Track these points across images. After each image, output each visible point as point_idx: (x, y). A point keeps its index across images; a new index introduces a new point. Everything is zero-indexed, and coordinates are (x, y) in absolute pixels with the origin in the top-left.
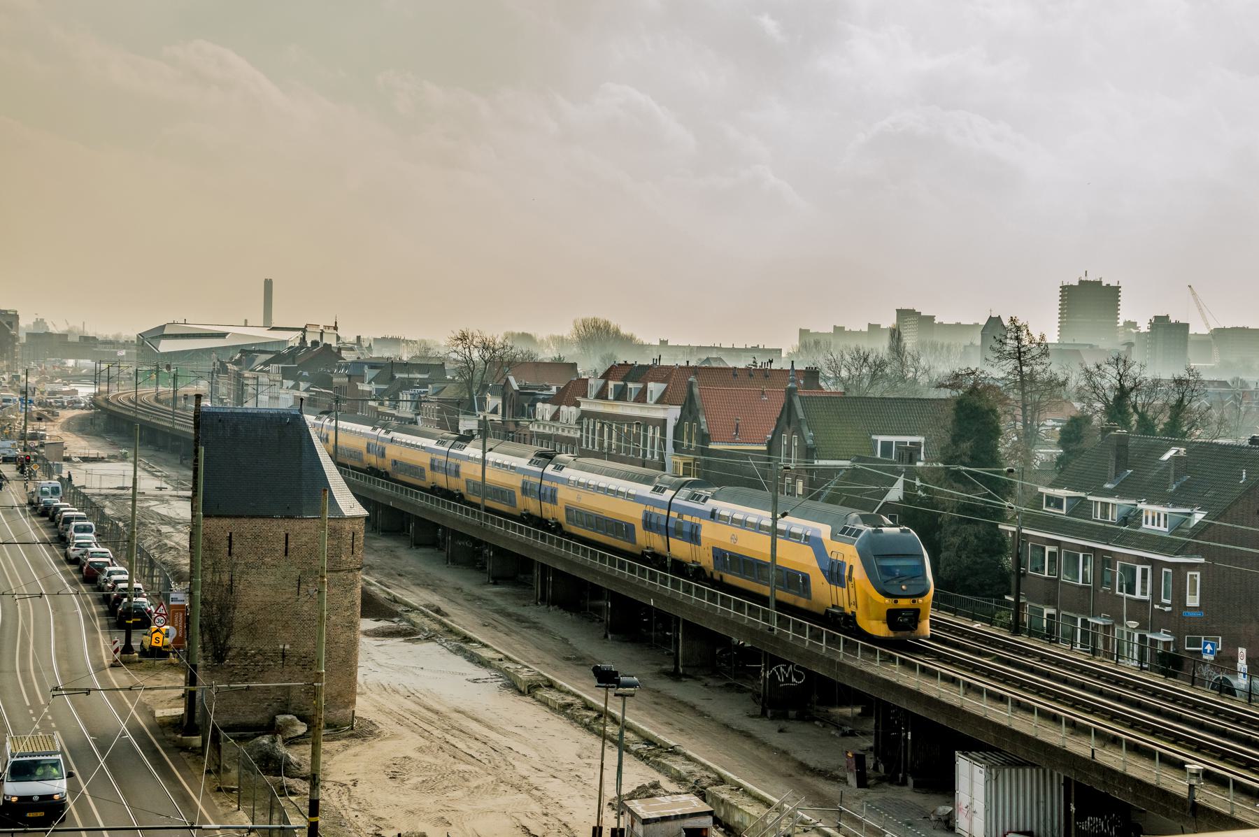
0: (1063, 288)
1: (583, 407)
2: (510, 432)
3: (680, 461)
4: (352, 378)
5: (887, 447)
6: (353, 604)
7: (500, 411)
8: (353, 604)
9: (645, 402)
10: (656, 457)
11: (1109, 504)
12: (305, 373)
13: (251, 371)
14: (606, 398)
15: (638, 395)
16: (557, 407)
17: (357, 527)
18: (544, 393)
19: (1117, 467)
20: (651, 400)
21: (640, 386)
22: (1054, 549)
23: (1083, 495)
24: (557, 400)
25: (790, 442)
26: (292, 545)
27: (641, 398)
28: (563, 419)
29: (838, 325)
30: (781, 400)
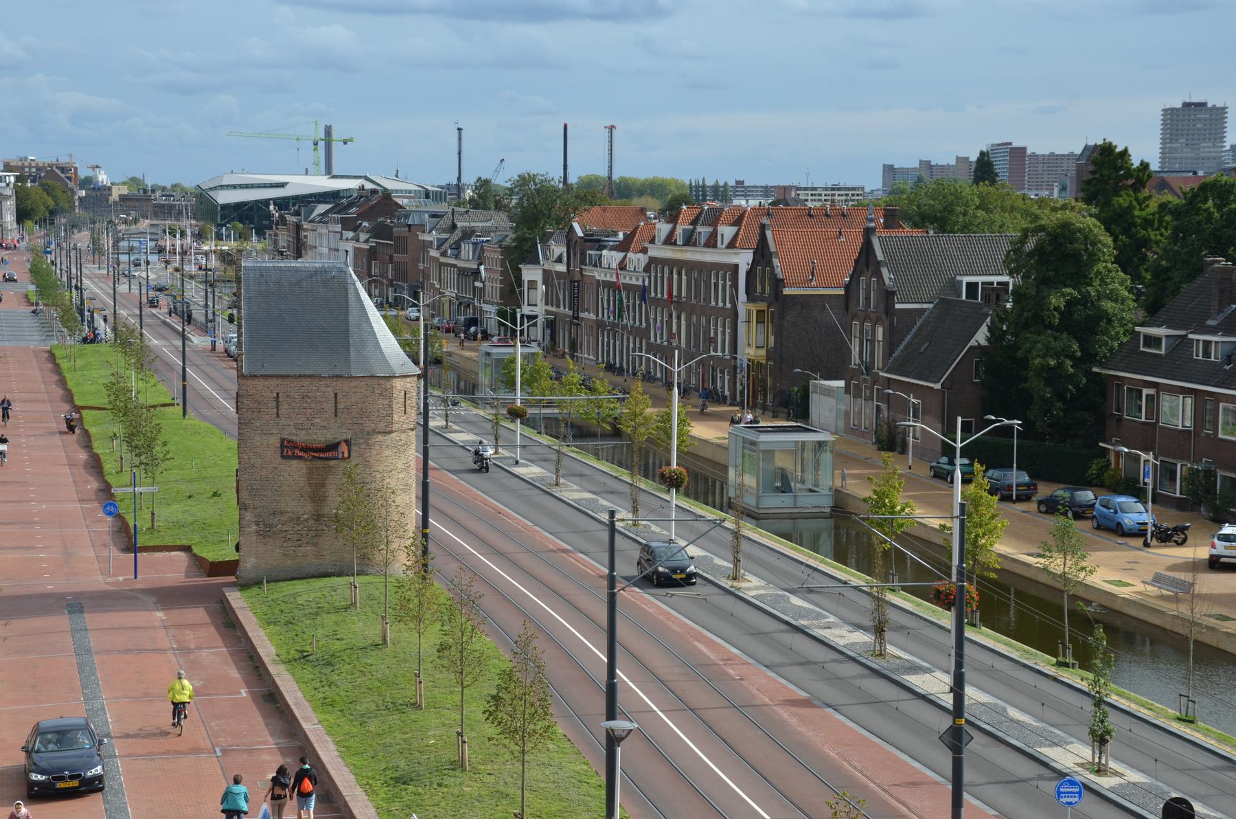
0: (1165, 110)
1: (650, 253)
2: (576, 282)
3: (754, 308)
4: (412, 228)
5: (972, 287)
6: (407, 465)
7: (565, 259)
8: (407, 465)
9: (715, 246)
10: (728, 305)
11: (1211, 342)
12: (365, 224)
13: (309, 222)
14: (675, 244)
15: (707, 240)
16: (624, 254)
17: (408, 385)
18: (610, 239)
19: (1220, 302)
20: (722, 244)
21: (710, 229)
22: (1152, 391)
23: (1183, 333)
24: (624, 246)
25: (869, 286)
26: (341, 406)
27: (711, 243)
28: (630, 267)
29: (960, 156)
30: (858, 242)
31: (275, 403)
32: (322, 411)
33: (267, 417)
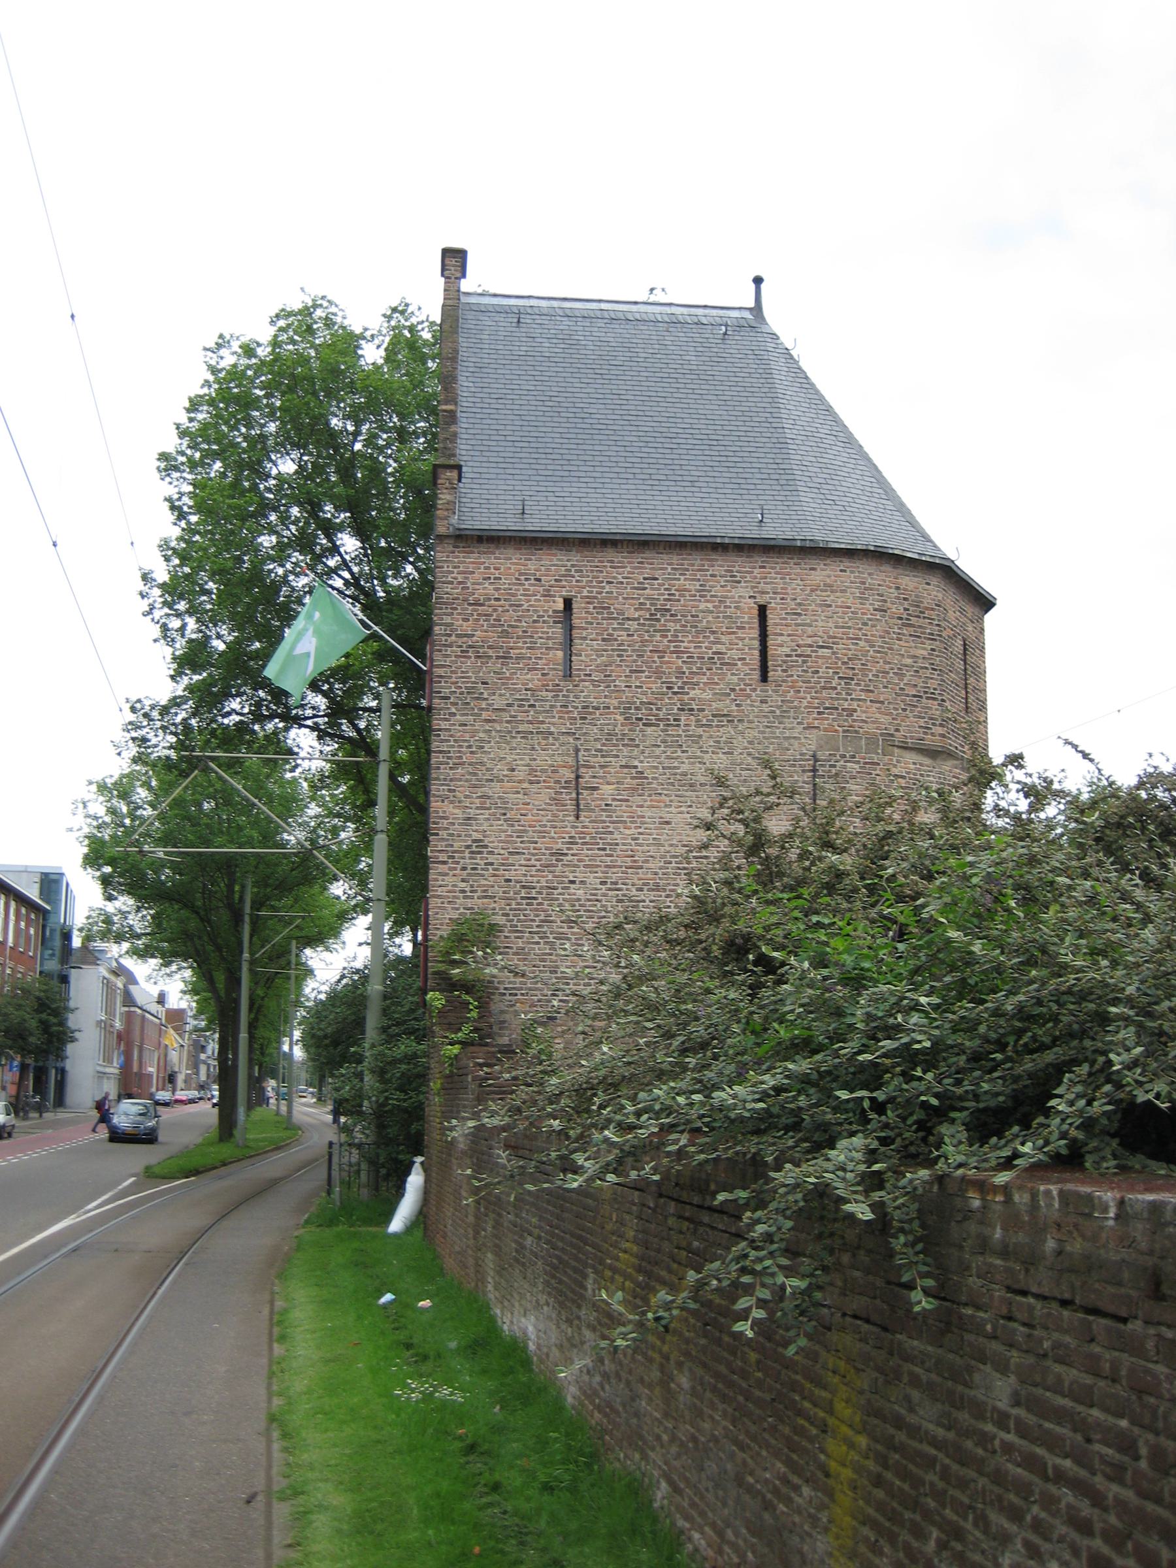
26: (779, 647)
31: (558, 630)
32: (719, 661)
33: (534, 679)
